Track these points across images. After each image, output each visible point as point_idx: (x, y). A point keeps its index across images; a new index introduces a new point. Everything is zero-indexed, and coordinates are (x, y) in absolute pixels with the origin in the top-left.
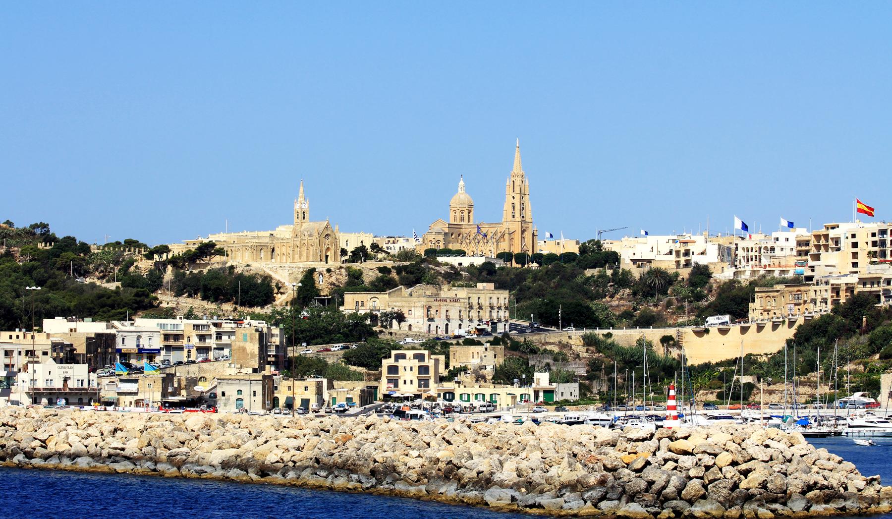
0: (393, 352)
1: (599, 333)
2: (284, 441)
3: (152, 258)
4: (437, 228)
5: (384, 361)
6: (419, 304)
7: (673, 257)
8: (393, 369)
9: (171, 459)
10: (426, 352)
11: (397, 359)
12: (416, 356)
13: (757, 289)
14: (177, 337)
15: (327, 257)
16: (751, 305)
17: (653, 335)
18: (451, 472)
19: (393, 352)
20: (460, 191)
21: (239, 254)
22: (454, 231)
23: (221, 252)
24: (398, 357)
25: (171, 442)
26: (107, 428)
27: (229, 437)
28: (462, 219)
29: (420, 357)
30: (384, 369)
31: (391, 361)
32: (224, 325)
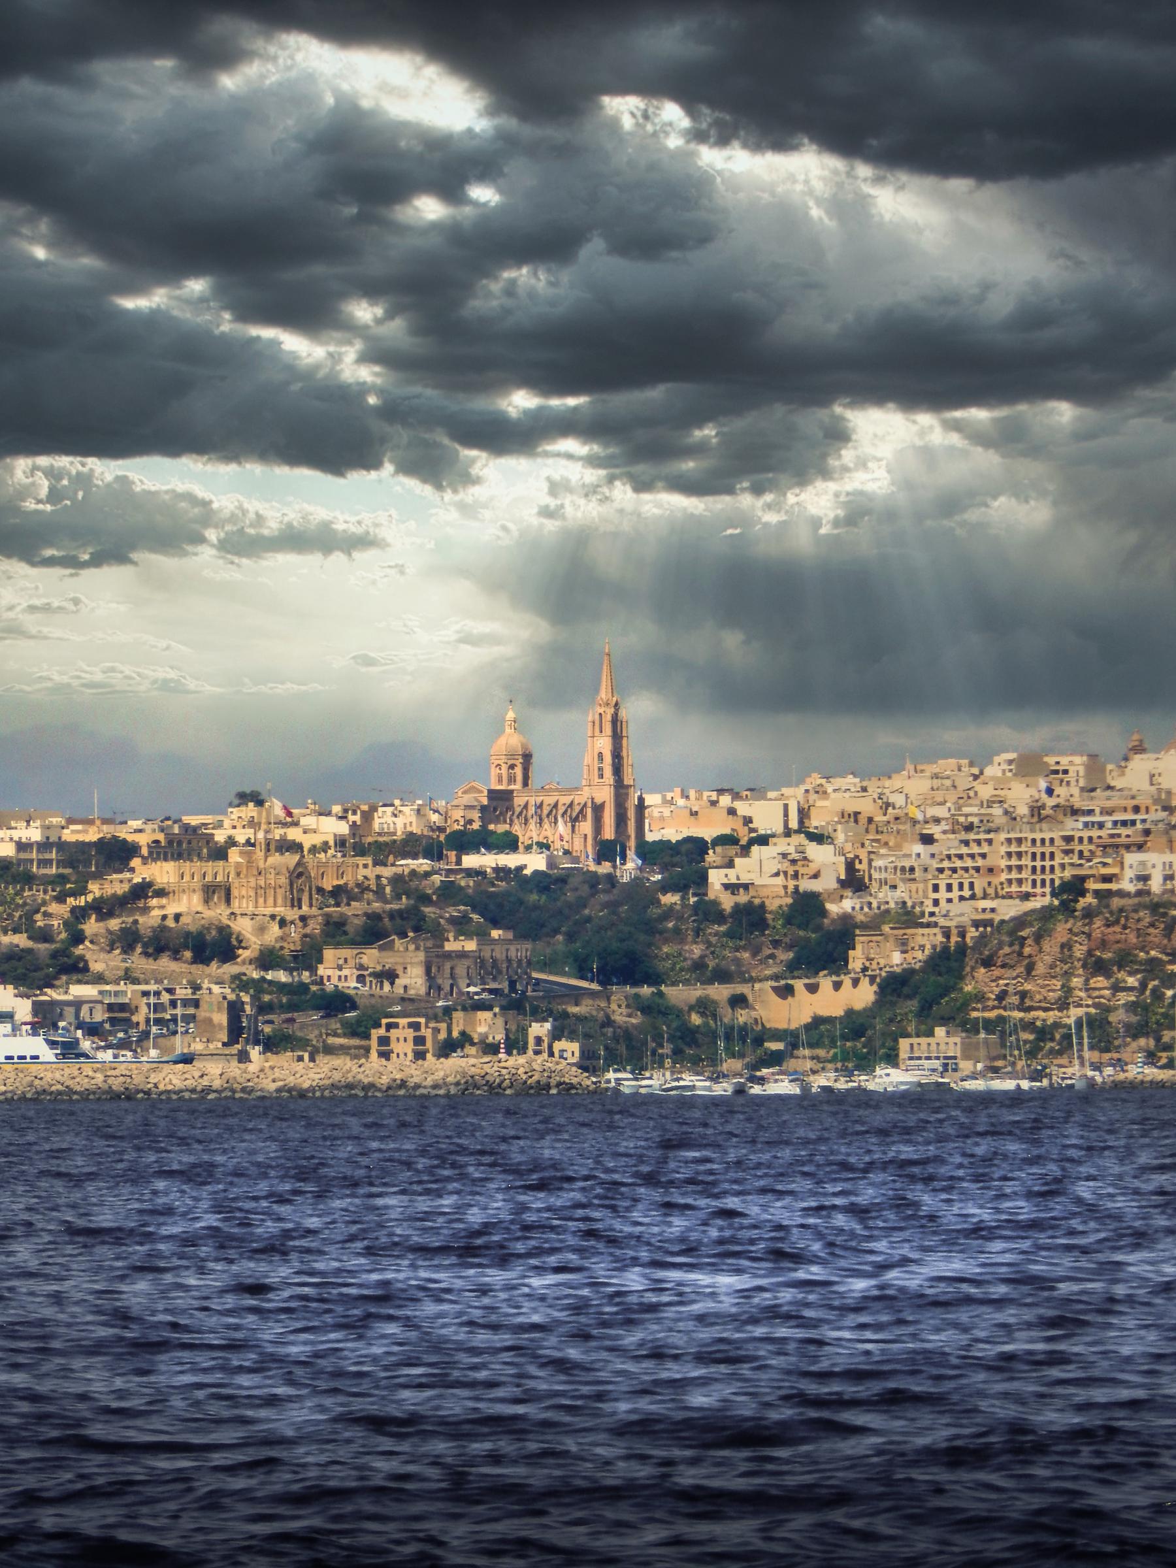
0: (384, 1021)
1: (646, 990)
2: (311, 1075)
3: (64, 902)
4: (468, 799)
5: (373, 1031)
6: (415, 960)
7: (780, 880)
8: (383, 1041)
9: (243, 1090)
10: (422, 1020)
11: (388, 1030)
12: (410, 1025)
13: (858, 932)
14: (123, 1007)
15: (300, 900)
16: (851, 952)
17: (720, 992)
18: (403, 1084)
19: (384, 1021)
20: (508, 730)
21: (185, 898)
22: (500, 802)
23: (161, 893)
24: (389, 1027)
25: (241, 1080)
26: (197, 1074)
27: (277, 1075)
28: (512, 779)
29: (416, 1026)
30: (374, 1043)
31: (382, 1031)
32: (178, 991)
